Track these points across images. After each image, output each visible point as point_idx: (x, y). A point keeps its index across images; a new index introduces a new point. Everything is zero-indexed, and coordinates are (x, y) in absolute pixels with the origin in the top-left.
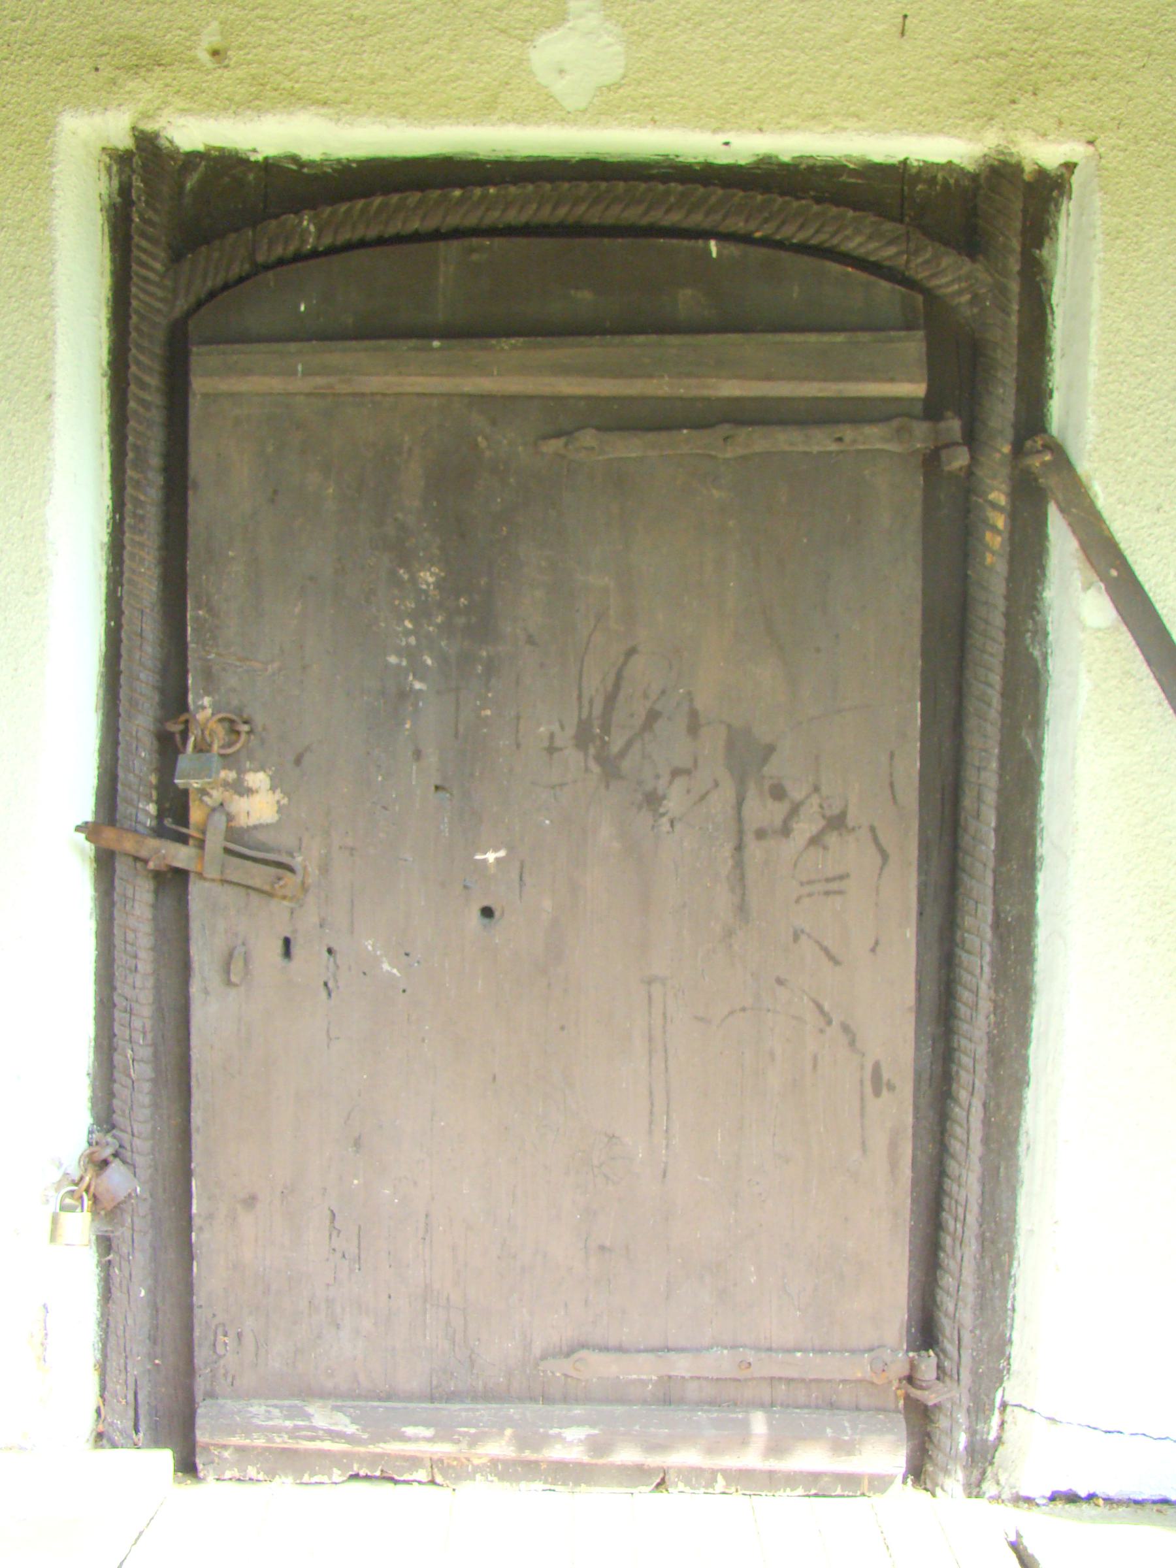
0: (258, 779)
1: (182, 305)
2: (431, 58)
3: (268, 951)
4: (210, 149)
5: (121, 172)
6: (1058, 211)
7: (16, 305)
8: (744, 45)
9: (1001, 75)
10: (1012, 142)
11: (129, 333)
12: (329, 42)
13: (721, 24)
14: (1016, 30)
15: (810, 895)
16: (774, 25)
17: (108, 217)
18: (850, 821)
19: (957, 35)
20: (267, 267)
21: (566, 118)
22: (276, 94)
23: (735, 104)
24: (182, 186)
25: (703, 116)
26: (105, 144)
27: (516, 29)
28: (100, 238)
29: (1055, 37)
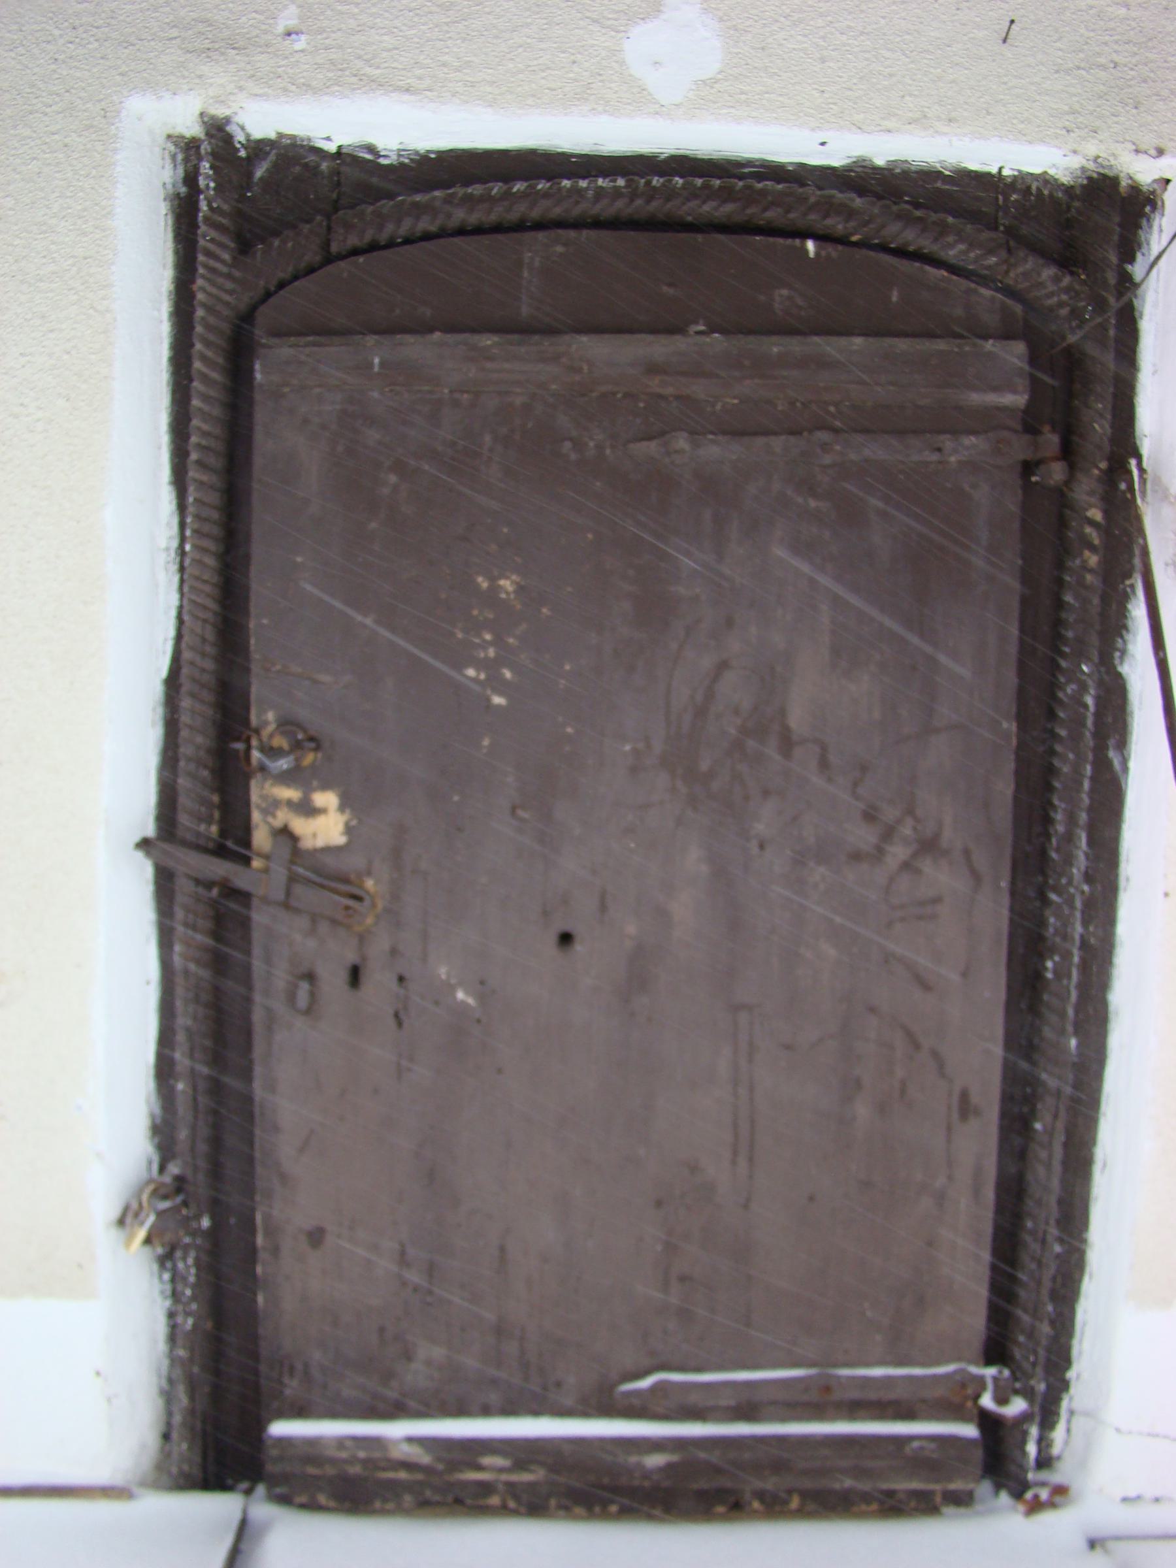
0: (326, 799)
1: (244, 301)
2: (521, 46)
3: (333, 980)
4: (281, 136)
5: (186, 160)
6: (1150, 227)
7: (75, 297)
8: (844, 45)
9: (1102, 87)
10: (1114, 155)
11: (193, 328)
12: (411, 27)
13: (820, 22)
14: (1116, 42)
15: (903, 919)
16: (875, 26)
17: (172, 206)
18: (944, 843)
19: (1058, 44)
20: (341, 257)
21: (661, 111)
22: (354, 80)
23: (835, 104)
24: (250, 175)
25: (801, 114)
26: (171, 132)
27: (609, 19)
28: (162, 228)
29: (1154, 51)
